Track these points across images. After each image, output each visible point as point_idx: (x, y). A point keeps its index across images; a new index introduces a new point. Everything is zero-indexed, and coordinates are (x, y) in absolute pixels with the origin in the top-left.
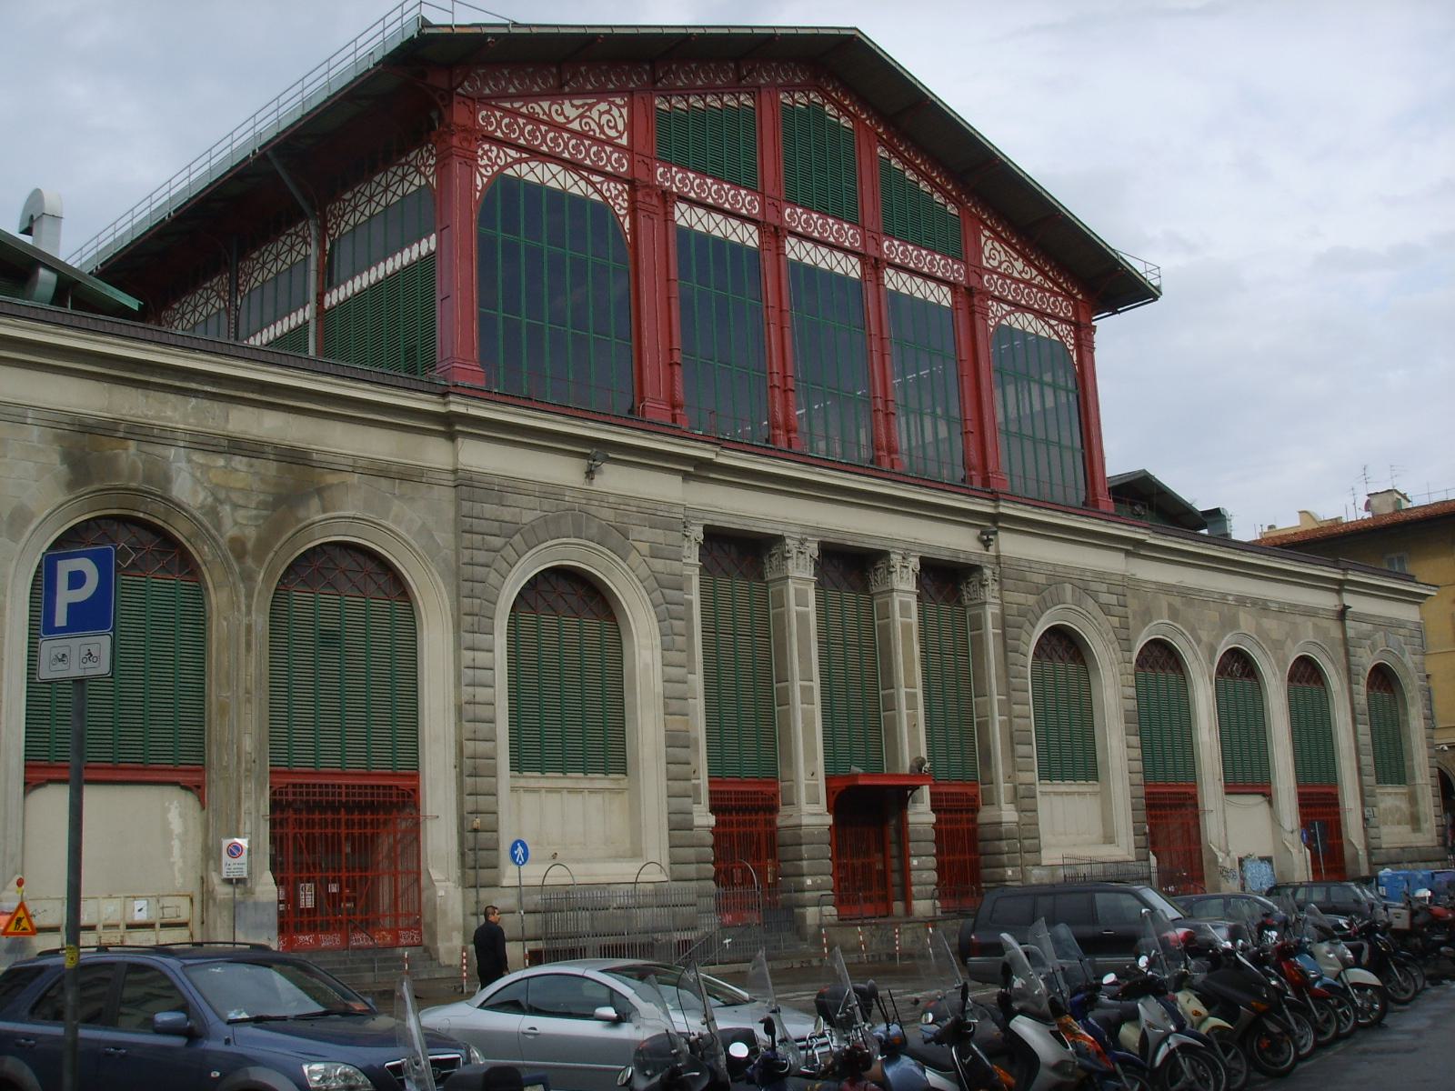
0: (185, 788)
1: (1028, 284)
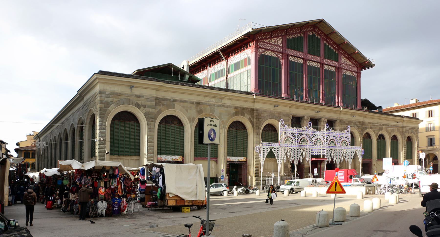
1: (349, 65)
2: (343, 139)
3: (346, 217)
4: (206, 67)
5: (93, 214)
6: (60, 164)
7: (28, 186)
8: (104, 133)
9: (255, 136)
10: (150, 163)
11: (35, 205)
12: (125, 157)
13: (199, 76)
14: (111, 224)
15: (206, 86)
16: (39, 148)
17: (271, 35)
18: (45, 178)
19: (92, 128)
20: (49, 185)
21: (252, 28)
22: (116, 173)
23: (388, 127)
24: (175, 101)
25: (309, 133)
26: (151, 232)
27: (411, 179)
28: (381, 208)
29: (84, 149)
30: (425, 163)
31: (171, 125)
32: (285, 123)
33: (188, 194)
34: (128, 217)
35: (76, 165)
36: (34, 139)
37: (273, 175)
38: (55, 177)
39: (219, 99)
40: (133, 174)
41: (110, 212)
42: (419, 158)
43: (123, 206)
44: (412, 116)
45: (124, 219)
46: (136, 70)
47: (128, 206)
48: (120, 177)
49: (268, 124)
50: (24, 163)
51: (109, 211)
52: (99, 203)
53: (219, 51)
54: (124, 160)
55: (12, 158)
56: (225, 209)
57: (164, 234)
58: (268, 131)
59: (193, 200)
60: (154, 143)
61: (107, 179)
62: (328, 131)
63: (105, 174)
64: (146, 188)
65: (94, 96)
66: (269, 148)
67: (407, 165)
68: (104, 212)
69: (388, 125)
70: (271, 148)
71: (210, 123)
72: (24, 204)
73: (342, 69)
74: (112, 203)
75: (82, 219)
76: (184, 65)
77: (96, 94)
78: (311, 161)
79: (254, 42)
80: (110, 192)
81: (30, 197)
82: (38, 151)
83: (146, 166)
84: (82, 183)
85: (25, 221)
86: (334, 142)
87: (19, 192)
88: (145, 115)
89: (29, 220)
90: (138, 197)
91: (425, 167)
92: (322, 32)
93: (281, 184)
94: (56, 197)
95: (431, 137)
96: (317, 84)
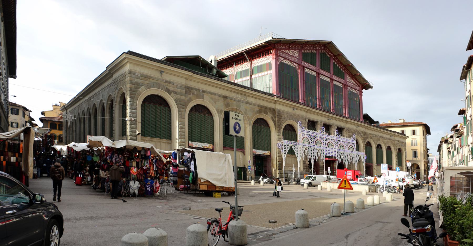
0: (242, 152)
1: (353, 84)
2: (350, 145)
3: (354, 209)
4: (232, 65)
5: (125, 193)
6: (89, 140)
7: (56, 160)
8: (135, 113)
9: (277, 134)
10: (181, 148)
11: (63, 179)
12: (157, 139)
13: (226, 72)
14: (144, 204)
15: (233, 83)
16: (66, 121)
17: (289, 47)
18: (74, 152)
19: (123, 107)
20: (78, 160)
21: (272, 37)
22: (148, 154)
23: (384, 139)
24: (204, 92)
25: (322, 136)
26: (184, 214)
27: (401, 182)
28: (380, 203)
29: (114, 127)
30: (411, 171)
31: (201, 114)
32: (302, 125)
33: (218, 180)
34: (161, 198)
35: (106, 142)
36: (61, 110)
37: (294, 170)
38: (84, 152)
39: (244, 96)
40: (165, 157)
41: (143, 192)
42: (407, 166)
43: (156, 188)
44: (401, 132)
45: (157, 200)
46: (166, 57)
47: (161, 187)
48: (152, 158)
49: (288, 125)
50: (50, 134)
51: (142, 192)
52: (132, 183)
53: (243, 52)
54: (156, 142)
55: (37, 127)
56: (252, 197)
57: (197, 217)
58: (288, 131)
59: (223, 187)
60: (185, 129)
61: (139, 159)
62: (338, 136)
63: (137, 154)
64: (178, 172)
65: (123, 75)
66: (289, 146)
67: (398, 171)
68: (137, 192)
69: (384, 138)
70: (291, 145)
71: (235, 117)
72: (51, 178)
73: (348, 86)
74: (145, 184)
75: (114, 198)
76: (212, 60)
77: (125, 73)
78: (325, 161)
79: (275, 50)
80: (142, 172)
81: (57, 170)
82: (66, 123)
83: (178, 150)
84: (113, 161)
85: (52, 196)
86: (343, 147)
87: (45, 164)
88: (176, 101)
89: (57, 195)
90: (171, 179)
91: (411, 174)
92: (332, 53)
93: (301, 178)
94: (86, 173)
95: (415, 151)
96: (328, 96)
